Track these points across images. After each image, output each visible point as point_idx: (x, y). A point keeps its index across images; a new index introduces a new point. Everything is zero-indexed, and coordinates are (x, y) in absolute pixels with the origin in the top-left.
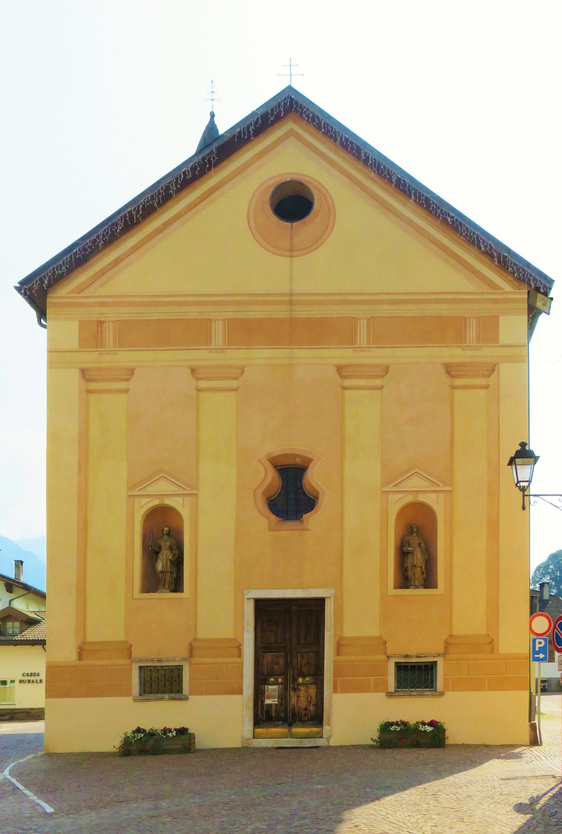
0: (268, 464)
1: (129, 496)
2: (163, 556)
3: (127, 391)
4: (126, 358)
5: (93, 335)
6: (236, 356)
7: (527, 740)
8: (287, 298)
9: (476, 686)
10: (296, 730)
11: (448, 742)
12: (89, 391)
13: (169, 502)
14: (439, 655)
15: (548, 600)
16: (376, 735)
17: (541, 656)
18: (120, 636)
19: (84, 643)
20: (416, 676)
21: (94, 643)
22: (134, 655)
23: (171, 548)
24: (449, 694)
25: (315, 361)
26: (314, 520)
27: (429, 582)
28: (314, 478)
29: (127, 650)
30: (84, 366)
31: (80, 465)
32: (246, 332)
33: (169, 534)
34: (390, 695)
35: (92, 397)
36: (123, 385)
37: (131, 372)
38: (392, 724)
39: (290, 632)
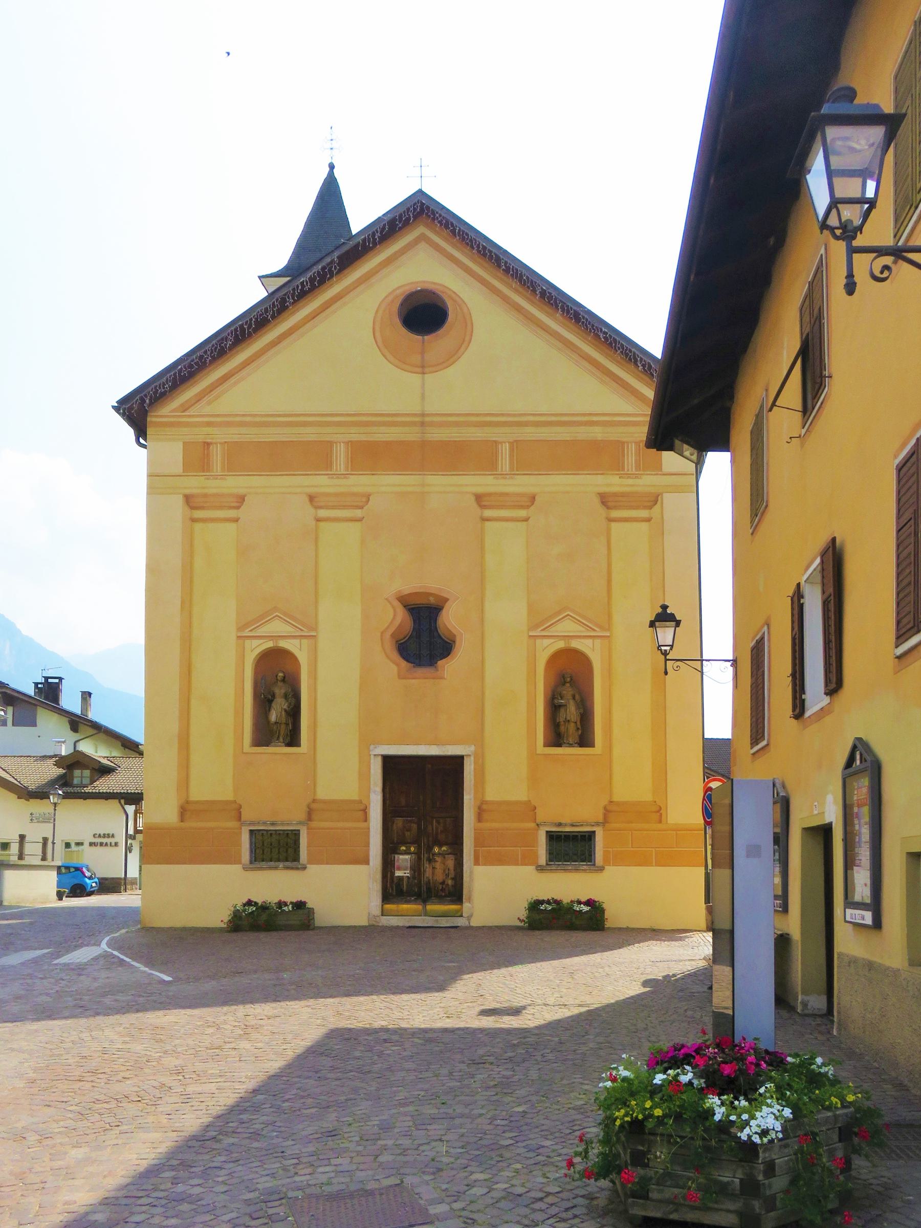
1: (239, 637)
2: (277, 706)
3: (236, 520)
4: (234, 484)
5: (198, 458)
6: (360, 482)
12: (194, 520)
13: (283, 644)
14: (597, 824)
16: (523, 914)
19: (187, 802)
22: (246, 815)
23: (286, 696)
24: (610, 870)
25: (451, 488)
26: (449, 667)
27: (585, 740)
28: (451, 619)
30: (187, 492)
31: (183, 602)
32: (371, 455)
33: (284, 680)
34: (540, 869)
35: (198, 526)
36: (232, 513)
37: (241, 499)
38: (542, 902)
39: (424, 798)
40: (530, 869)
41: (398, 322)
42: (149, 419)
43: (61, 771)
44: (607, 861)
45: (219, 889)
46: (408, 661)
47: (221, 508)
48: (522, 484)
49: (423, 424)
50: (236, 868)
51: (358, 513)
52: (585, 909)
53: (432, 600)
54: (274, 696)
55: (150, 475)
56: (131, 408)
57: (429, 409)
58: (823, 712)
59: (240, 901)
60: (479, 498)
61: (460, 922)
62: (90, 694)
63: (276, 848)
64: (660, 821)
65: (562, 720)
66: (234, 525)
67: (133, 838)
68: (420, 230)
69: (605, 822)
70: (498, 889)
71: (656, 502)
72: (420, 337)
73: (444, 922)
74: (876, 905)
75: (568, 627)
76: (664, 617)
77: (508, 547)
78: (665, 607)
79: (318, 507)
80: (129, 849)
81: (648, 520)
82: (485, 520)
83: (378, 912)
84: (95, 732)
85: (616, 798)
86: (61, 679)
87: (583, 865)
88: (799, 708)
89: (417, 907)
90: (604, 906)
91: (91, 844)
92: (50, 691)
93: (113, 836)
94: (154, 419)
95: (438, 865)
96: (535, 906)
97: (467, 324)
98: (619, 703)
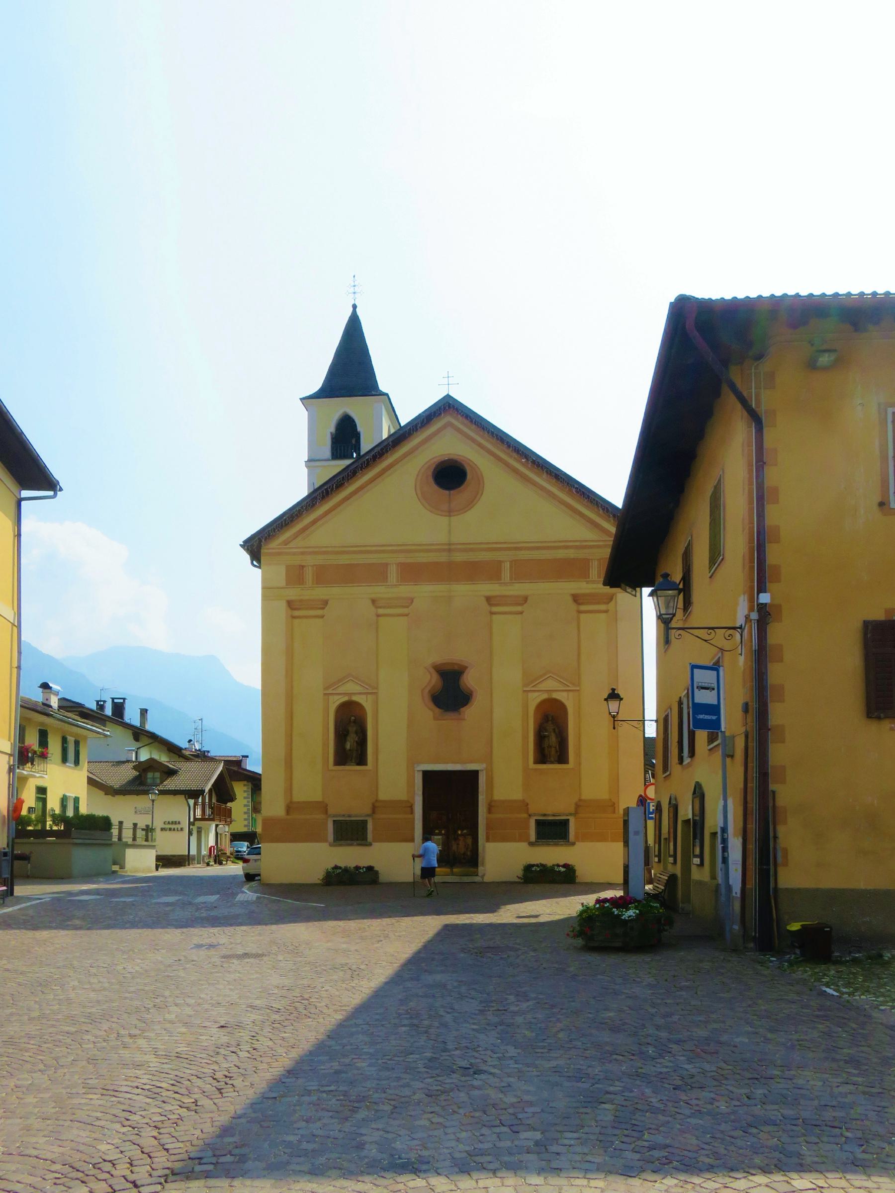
0: (432, 670)
2: (351, 737)
3: (322, 617)
4: (320, 592)
5: (296, 576)
6: (405, 590)
8: (446, 547)
12: (293, 617)
13: (355, 698)
14: (571, 814)
16: (520, 873)
18: (317, 796)
19: (291, 802)
21: (299, 802)
22: (331, 811)
23: (356, 733)
25: (468, 593)
26: (470, 712)
28: (470, 680)
29: (323, 807)
30: (289, 598)
32: (413, 572)
33: (355, 722)
34: (531, 844)
36: (320, 612)
37: (326, 603)
38: (533, 866)
39: (451, 800)
40: (524, 845)
41: (431, 480)
42: (262, 551)
43: (136, 773)
44: (577, 838)
45: (312, 859)
46: (439, 708)
47: (312, 609)
50: (324, 845)
51: (406, 611)
52: (563, 869)
53: (456, 668)
54: (348, 732)
55: (263, 588)
56: (252, 545)
57: (445, 519)
59: (330, 866)
60: (488, 599)
61: (477, 879)
62: (146, 710)
63: (351, 831)
64: (614, 812)
65: (546, 746)
66: (321, 620)
67: (194, 825)
68: (446, 419)
69: (576, 814)
70: (502, 858)
71: (611, 599)
72: (447, 492)
73: (466, 879)
75: (550, 684)
76: (614, 696)
77: (508, 630)
78: (613, 690)
79: (377, 607)
80: (190, 833)
81: (606, 611)
82: (492, 613)
84: (151, 741)
85: (583, 797)
86: (124, 699)
87: (561, 842)
88: (681, 760)
90: (576, 868)
91: (162, 829)
92: (119, 708)
93: (179, 823)
94: (266, 551)
95: (461, 843)
96: (528, 868)
97: (480, 480)
98: (586, 730)
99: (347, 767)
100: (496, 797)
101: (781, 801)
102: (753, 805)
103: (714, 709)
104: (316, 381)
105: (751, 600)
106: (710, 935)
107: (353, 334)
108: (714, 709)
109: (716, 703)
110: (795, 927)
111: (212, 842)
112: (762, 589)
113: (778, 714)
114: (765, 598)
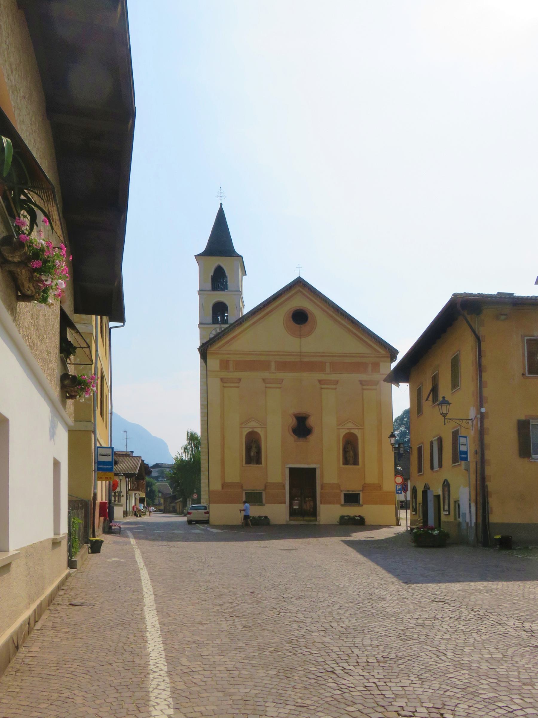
0: (293, 417)
1: (240, 427)
2: (253, 451)
3: (238, 387)
5: (225, 365)
6: (280, 375)
7: (395, 524)
8: (299, 354)
9: (376, 503)
10: (306, 518)
11: (366, 523)
12: (224, 387)
13: (255, 430)
14: (361, 491)
15: (403, 454)
16: (338, 520)
17: (400, 492)
19: (224, 483)
20: (352, 499)
22: (244, 488)
23: (256, 447)
24: (364, 506)
25: (310, 378)
26: (312, 438)
27: (356, 463)
28: (311, 422)
32: (283, 366)
33: (255, 441)
34: (342, 505)
36: (237, 385)
37: (240, 380)
38: (345, 516)
39: (303, 481)
40: (339, 506)
48: (334, 377)
49: (301, 356)
53: (304, 415)
58: (437, 471)
60: (320, 381)
61: (317, 523)
68: (298, 288)
69: (362, 491)
70: (329, 512)
74: (449, 510)
75: (350, 425)
82: (322, 388)
83: (288, 519)
89: (301, 518)
96: (342, 517)
99: (252, 465)
100: (325, 482)
101: (489, 489)
102: (479, 490)
103: (466, 453)
104: (202, 247)
105: (477, 410)
106: (461, 541)
107: (221, 221)
108: (466, 453)
109: (466, 450)
110: (498, 537)
111: (133, 504)
112: (481, 406)
113: (488, 455)
114: (483, 410)
